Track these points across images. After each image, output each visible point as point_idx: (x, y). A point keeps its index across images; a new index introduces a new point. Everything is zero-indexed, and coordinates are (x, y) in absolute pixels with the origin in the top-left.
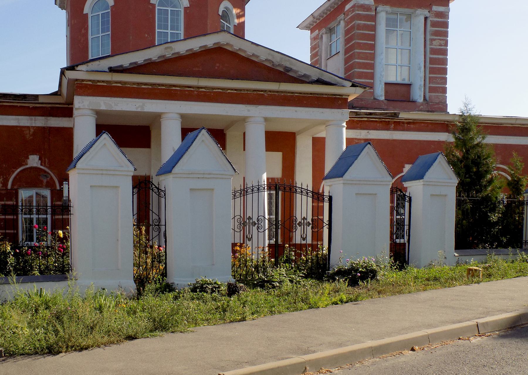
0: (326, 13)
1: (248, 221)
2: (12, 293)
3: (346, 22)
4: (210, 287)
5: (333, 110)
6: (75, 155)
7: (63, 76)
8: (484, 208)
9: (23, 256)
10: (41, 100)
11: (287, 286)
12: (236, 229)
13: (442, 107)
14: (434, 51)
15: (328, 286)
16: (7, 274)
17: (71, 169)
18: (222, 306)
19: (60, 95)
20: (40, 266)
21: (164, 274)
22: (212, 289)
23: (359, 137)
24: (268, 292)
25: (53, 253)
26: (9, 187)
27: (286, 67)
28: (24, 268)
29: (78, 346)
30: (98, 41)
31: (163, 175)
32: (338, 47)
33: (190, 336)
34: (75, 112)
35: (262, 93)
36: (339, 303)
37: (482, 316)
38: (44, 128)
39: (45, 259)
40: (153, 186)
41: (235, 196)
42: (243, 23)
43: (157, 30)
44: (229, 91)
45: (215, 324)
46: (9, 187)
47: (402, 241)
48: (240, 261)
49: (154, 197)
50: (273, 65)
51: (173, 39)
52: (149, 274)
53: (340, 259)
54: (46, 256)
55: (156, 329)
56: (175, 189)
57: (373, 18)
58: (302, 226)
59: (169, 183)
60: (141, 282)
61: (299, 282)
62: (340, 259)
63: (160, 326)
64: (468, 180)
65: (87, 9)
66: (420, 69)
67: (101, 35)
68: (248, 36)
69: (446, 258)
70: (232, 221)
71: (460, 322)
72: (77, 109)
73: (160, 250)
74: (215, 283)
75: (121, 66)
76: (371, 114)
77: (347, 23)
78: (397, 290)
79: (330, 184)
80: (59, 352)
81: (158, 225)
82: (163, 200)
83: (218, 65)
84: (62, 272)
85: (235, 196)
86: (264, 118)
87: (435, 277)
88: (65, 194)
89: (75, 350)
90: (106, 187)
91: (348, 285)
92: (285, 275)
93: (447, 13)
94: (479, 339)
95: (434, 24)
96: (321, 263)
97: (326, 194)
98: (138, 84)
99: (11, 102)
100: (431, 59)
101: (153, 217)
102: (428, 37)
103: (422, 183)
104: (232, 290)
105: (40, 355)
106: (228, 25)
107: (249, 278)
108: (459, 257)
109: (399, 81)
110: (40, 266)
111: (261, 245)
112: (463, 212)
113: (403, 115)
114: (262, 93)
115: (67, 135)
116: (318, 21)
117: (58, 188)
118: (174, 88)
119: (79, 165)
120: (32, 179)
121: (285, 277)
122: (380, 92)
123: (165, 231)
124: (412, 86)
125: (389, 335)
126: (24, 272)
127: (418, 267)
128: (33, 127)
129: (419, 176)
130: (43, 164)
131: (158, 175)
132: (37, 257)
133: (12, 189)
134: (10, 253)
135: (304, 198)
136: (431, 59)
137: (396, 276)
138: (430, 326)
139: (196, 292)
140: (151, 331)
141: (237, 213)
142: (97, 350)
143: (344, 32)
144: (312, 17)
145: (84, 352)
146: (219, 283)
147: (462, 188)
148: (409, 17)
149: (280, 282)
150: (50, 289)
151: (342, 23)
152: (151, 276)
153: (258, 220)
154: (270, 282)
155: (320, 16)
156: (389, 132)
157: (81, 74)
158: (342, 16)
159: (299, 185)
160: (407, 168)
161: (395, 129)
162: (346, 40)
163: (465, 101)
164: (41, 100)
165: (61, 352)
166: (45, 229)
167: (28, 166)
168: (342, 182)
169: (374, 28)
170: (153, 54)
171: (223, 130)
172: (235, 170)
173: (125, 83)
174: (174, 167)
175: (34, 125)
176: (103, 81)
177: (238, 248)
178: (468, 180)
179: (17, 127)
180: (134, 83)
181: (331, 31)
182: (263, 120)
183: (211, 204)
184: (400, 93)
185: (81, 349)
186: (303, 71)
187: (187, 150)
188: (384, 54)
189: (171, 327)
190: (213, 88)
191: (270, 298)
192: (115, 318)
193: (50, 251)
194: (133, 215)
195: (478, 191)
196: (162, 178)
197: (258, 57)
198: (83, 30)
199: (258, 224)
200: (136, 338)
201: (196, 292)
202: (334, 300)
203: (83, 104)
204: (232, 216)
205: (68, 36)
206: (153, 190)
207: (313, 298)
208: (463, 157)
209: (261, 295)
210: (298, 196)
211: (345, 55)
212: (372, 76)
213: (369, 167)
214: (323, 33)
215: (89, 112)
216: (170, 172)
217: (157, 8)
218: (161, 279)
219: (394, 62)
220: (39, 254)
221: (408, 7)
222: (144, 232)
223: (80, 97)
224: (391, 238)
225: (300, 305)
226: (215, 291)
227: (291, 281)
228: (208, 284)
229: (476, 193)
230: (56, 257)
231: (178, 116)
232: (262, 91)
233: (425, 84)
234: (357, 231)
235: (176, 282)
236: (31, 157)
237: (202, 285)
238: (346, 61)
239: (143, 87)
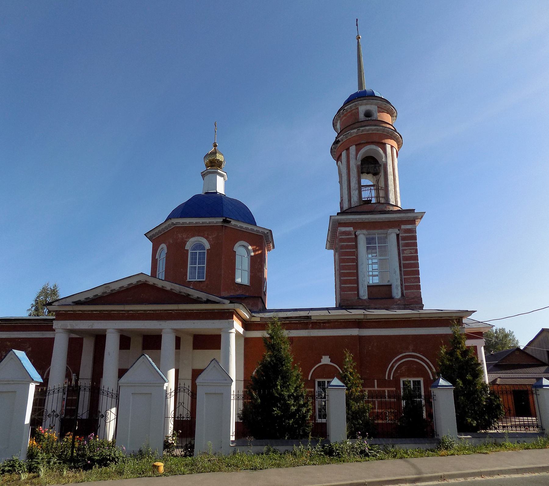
43: (205, 265)
75: (80, 301)
95: (404, 239)
100: (404, 264)
122: (364, 294)
135: (110, 399)
159: (106, 389)
161: (313, 328)
173: (84, 311)
210: (105, 397)
212: (357, 282)
221: (381, 228)
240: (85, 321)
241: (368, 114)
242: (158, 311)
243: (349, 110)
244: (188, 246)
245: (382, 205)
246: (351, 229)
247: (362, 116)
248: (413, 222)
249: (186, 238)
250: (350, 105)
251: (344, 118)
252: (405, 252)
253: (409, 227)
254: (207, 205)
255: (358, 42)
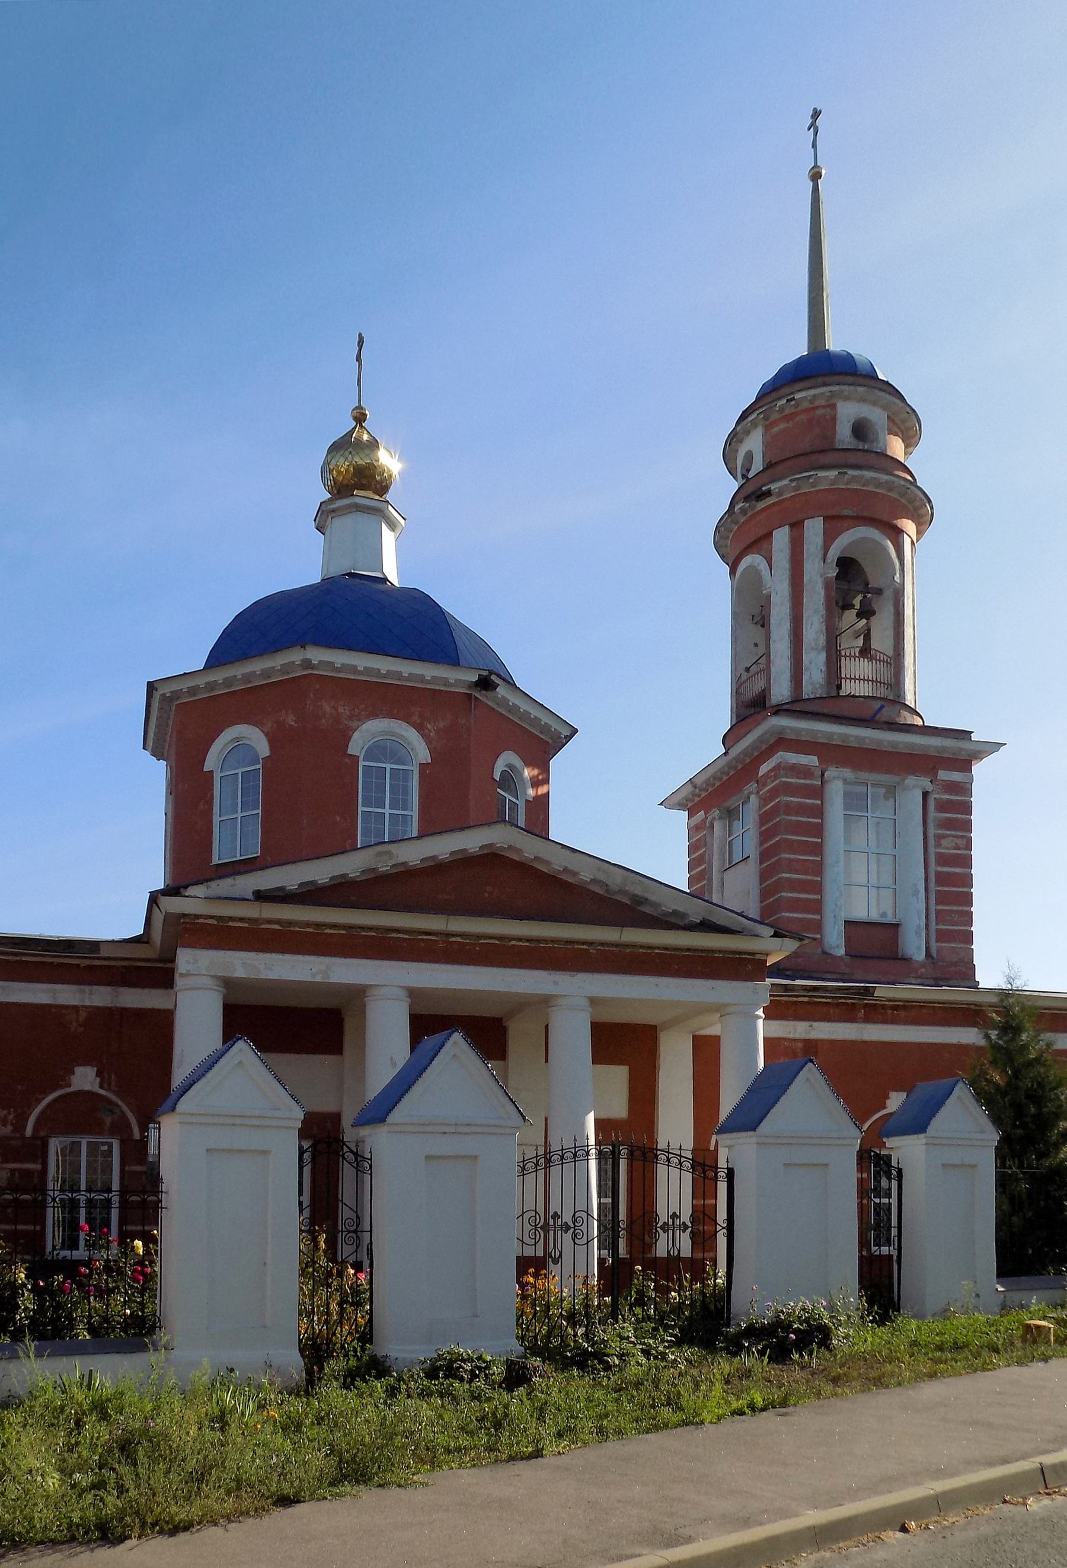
0: (720, 779)
1: (551, 1222)
2: (25, 1382)
3: (760, 798)
4: (468, 1367)
5: (735, 984)
6: (179, 1076)
7: (155, 908)
8: (1055, 1190)
9: (53, 1295)
10: (104, 952)
11: (638, 1365)
12: (526, 1239)
13: (965, 971)
14: (944, 860)
15: (724, 1365)
16: (17, 1336)
17: (164, 1113)
18: (494, 1414)
19: (147, 942)
20: (90, 1317)
21: (366, 1336)
22: (472, 1370)
23: (791, 1036)
24: (594, 1379)
25: (121, 1285)
26: (29, 1131)
27: (637, 896)
28: (53, 1322)
29: (167, 1523)
30: (235, 831)
31: (366, 1127)
32: (745, 849)
33: (417, 1496)
34: (179, 982)
35: (585, 947)
36: (747, 1411)
37: (1050, 1447)
38: (110, 1009)
39: (102, 1298)
40: (345, 1149)
41: (523, 1168)
42: (547, 795)
43: (360, 809)
44: (513, 943)
45: (474, 1466)
46: (29, 1131)
47: (885, 1250)
48: (534, 1305)
49: (347, 1172)
50: (607, 891)
51: (392, 831)
52: (334, 1334)
53: (755, 1300)
54: (104, 1293)
55: (345, 1477)
56: (396, 1163)
57: (819, 792)
58: (671, 1232)
59: (383, 1144)
60: (315, 1352)
61: (663, 1354)
62: (755, 1300)
63: (354, 1471)
64: (1019, 1131)
65: (211, 762)
66: (916, 893)
67: (239, 815)
68: (556, 833)
69: (978, 1295)
70: (517, 1223)
71: (1005, 1461)
72: (182, 975)
73: (358, 1278)
74: (480, 1358)
75: (282, 889)
76: (815, 989)
77: (764, 800)
78: (873, 1374)
79: (728, 1142)
80: (122, 1539)
81: (355, 1232)
82: (367, 1177)
83: (489, 888)
84: (139, 1331)
85: (523, 1168)
86: (588, 997)
87: (955, 1343)
88: (152, 1150)
89: (161, 1532)
90: (241, 1151)
91: (769, 1363)
92: (633, 1339)
93: (968, 786)
94: (1046, 1501)
95: (942, 806)
96: (712, 1307)
97: (722, 1163)
98: (318, 925)
99: (37, 955)
100: (938, 875)
101: (346, 1214)
102: (932, 831)
103: (924, 1141)
104: (516, 1377)
105: (81, 1544)
106: (514, 800)
107: (555, 1346)
108: (1007, 1294)
109: (875, 916)
110: (90, 1317)
111: (581, 1272)
112: (1012, 1199)
113: (883, 992)
114: (585, 947)
115: (160, 1027)
116: (704, 794)
117: (137, 1135)
118: (394, 935)
119: (183, 1105)
120: (79, 1114)
121: (633, 1342)
122: (835, 940)
123: (371, 1243)
124: (901, 930)
125: (854, 1494)
126: (52, 1332)
127: (919, 1316)
128: (86, 1007)
129: (916, 1123)
130: (105, 1085)
131: (359, 1123)
132: (84, 1298)
133: (34, 1137)
134: (24, 1285)
135: (675, 1172)
136: (938, 875)
137: (872, 1338)
138: (939, 1474)
139: (437, 1378)
140: (332, 1484)
141: (529, 1205)
142: (212, 1533)
143: (757, 818)
144: (690, 785)
145: (182, 1537)
146: (489, 1358)
147: (1006, 1151)
148: (891, 791)
149: (621, 1356)
150: (112, 1372)
151: (753, 799)
152: (340, 1348)
153: (574, 1221)
154: (599, 1356)
155: (707, 782)
156: (855, 1025)
157: (195, 902)
158: (753, 786)
159: (662, 1144)
160: (895, 1101)
161: (867, 1020)
162: (761, 834)
163: (1007, 971)
164: (104, 952)
165: (129, 1537)
166: (104, 1233)
167: (71, 1089)
168: (754, 1140)
169: (819, 812)
170: (349, 865)
171: (501, 1019)
172: (524, 1118)
173: (290, 923)
174: (390, 1110)
175: (88, 1004)
176: (241, 920)
177: (531, 1280)
178: (1019, 1131)
179: (50, 1006)
180: (308, 924)
181: (731, 814)
182: (585, 1003)
183: (473, 1181)
184: (875, 943)
185: (176, 1529)
186: (671, 905)
187: (420, 1075)
188: (842, 864)
189: (376, 1474)
190: (479, 937)
191: (599, 1394)
192: (257, 1447)
193: (116, 1282)
194: (301, 1211)
195: (1041, 1156)
196: (364, 1132)
197: (575, 874)
198: (201, 803)
199: (574, 1228)
200: (299, 1502)
201: (437, 1378)
202: (735, 1405)
203: (196, 965)
204: (517, 1212)
205: (169, 815)
206: (344, 1158)
207: (688, 1399)
208: (1008, 1084)
209: (579, 1384)
210: (661, 1170)
211: (761, 863)
212: (817, 907)
213: (811, 1105)
214: (714, 818)
215: (209, 982)
216: (382, 1120)
217: (361, 764)
218: (359, 1349)
219: (863, 880)
220: (88, 1292)
221: (888, 771)
222: (323, 1245)
223: (189, 951)
224: (863, 1243)
225: (666, 1413)
226: (478, 1376)
227: (646, 1353)
228: (464, 1361)
229: (1038, 1159)
230: (126, 1293)
231: (402, 993)
232: (584, 943)
233: (927, 925)
234: (787, 1243)
235: (393, 1355)
236: (79, 1070)
237: (451, 1362)
238: (764, 876)
239: (328, 931)
240: (300, 957)
241: (860, 430)
242: (546, 941)
243: (806, 405)
244: (357, 745)
245: (887, 707)
246: (812, 760)
247: (844, 433)
248: (965, 764)
249: (350, 718)
250: (813, 392)
251: (782, 426)
252: (944, 842)
253: (956, 776)
254: (353, 611)
255: (816, 190)
